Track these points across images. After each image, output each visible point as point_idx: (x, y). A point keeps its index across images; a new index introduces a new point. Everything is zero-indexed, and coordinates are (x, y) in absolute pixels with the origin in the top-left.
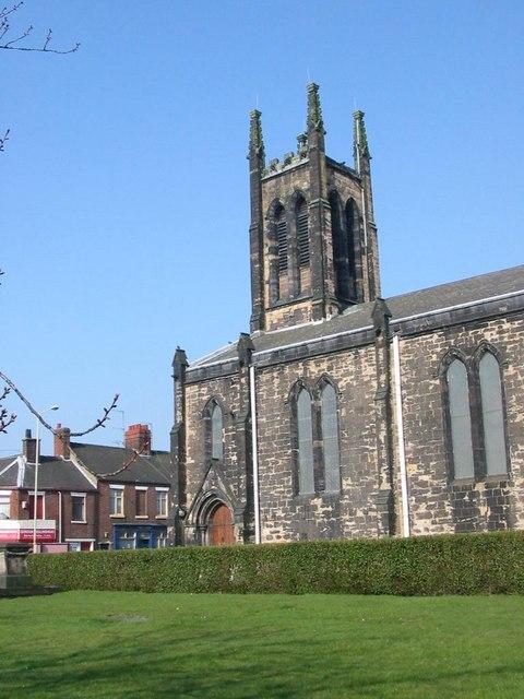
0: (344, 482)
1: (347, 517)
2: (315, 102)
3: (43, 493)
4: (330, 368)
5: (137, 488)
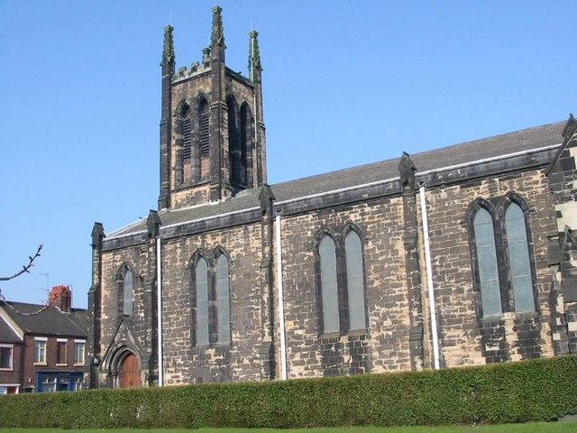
0: (233, 336)
1: (236, 364)
2: (218, 21)
4: (224, 241)
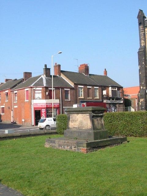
3: (54, 89)
5: (88, 87)
